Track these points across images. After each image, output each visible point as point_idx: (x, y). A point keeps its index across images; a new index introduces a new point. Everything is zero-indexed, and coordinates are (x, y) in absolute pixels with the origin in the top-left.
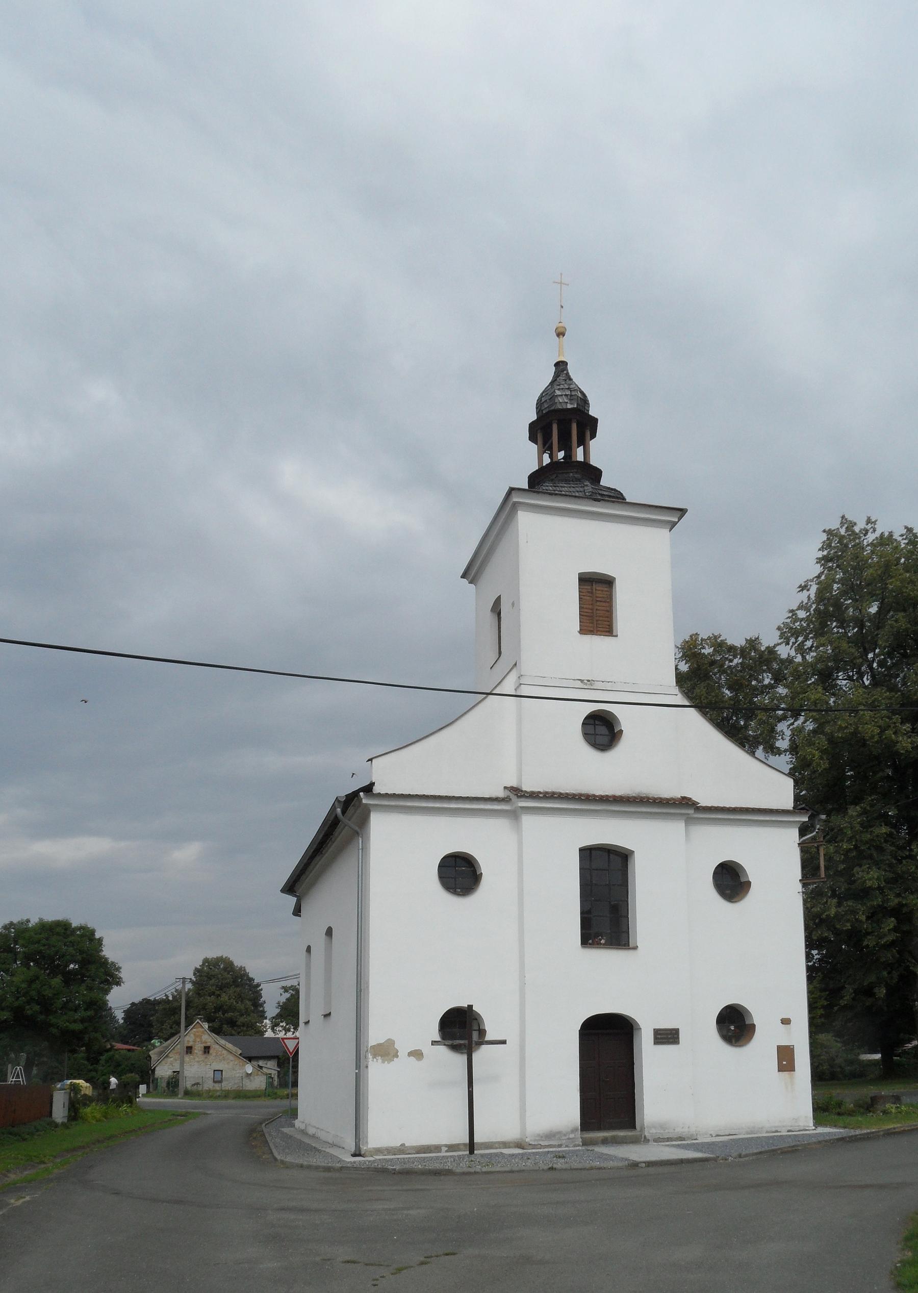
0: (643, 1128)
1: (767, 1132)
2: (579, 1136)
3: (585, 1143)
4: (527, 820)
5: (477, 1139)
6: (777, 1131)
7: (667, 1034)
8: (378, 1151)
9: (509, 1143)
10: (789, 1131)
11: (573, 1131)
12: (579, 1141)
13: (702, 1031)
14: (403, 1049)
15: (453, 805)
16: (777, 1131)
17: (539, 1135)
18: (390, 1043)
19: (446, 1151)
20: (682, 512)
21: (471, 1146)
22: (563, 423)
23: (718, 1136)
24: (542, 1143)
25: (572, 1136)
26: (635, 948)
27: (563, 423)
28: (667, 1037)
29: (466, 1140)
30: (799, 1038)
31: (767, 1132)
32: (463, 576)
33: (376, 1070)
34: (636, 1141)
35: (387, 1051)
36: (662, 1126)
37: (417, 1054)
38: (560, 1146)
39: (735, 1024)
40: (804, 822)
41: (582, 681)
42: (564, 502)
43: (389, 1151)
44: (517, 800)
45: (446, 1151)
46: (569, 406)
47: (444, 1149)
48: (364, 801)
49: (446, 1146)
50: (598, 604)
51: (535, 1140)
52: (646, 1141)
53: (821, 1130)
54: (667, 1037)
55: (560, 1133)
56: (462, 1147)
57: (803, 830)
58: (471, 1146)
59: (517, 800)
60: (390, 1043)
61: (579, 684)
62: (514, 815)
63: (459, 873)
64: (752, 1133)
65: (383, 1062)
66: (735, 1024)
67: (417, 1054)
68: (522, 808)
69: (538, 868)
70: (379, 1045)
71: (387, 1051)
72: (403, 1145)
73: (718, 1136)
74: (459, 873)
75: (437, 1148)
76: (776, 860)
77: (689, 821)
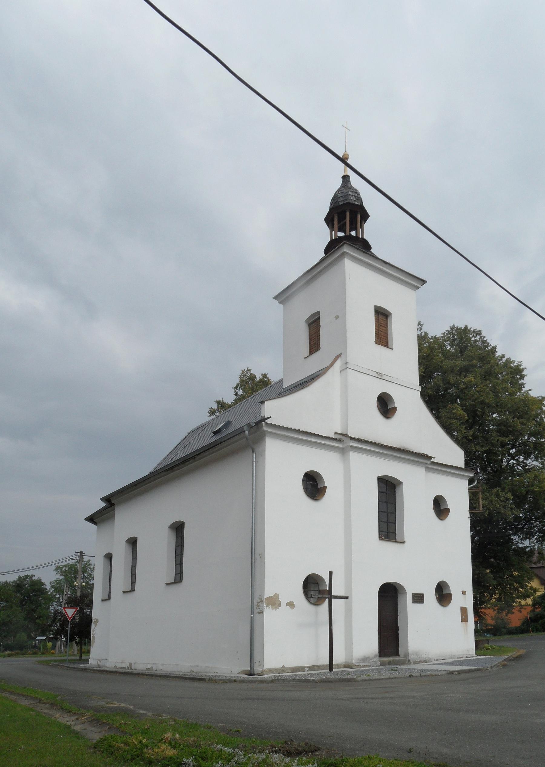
0: (406, 655)
1: (458, 658)
2: (378, 660)
3: (382, 664)
4: (354, 456)
5: (334, 662)
6: (461, 658)
7: (419, 597)
8: (271, 671)
9: (341, 665)
10: (467, 657)
11: (375, 657)
12: (379, 663)
13: (430, 596)
14: (284, 600)
15: (313, 439)
16: (461, 658)
17: (358, 659)
18: (276, 596)
19: (308, 671)
20: (424, 282)
21: (331, 666)
22: (346, 215)
23: (437, 660)
24: (362, 664)
25: (374, 660)
26: (403, 542)
27: (346, 215)
28: (419, 598)
29: (328, 663)
30: (469, 603)
31: (458, 658)
32: (276, 298)
33: (270, 616)
34: (403, 663)
35: (274, 602)
36: (417, 654)
37: (291, 605)
38: (370, 666)
39: (443, 594)
40: (471, 477)
41: (377, 373)
42: (368, 259)
43: (276, 670)
44: (342, 442)
45: (308, 671)
46: (356, 203)
47: (307, 669)
48: (265, 428)
49: (308, 667)
50: (381, 327)
51: (357, 663)
52: (409, 662)
53: (479, 657)
54: (419, 598)
55: (368, 658)
56: (316, 668)
57: (471, 481)
58: (331, 666)
59: (342, 442)
60: (276, 596)
61: (376, 375)
62: (343, 451)
63: (313, 486)
64: (451, 658)
65: (273, 609)
66: (464, 593)
67: (291, 605)
68: (352, 447)
69: (354, 481)
70: (271, 597)
71: (274, 602)
72: (283, 666)
73: (437, 660)
74: (313, 486)
75: (303, 669)
76: (458, 493)
77: (427, 469)
